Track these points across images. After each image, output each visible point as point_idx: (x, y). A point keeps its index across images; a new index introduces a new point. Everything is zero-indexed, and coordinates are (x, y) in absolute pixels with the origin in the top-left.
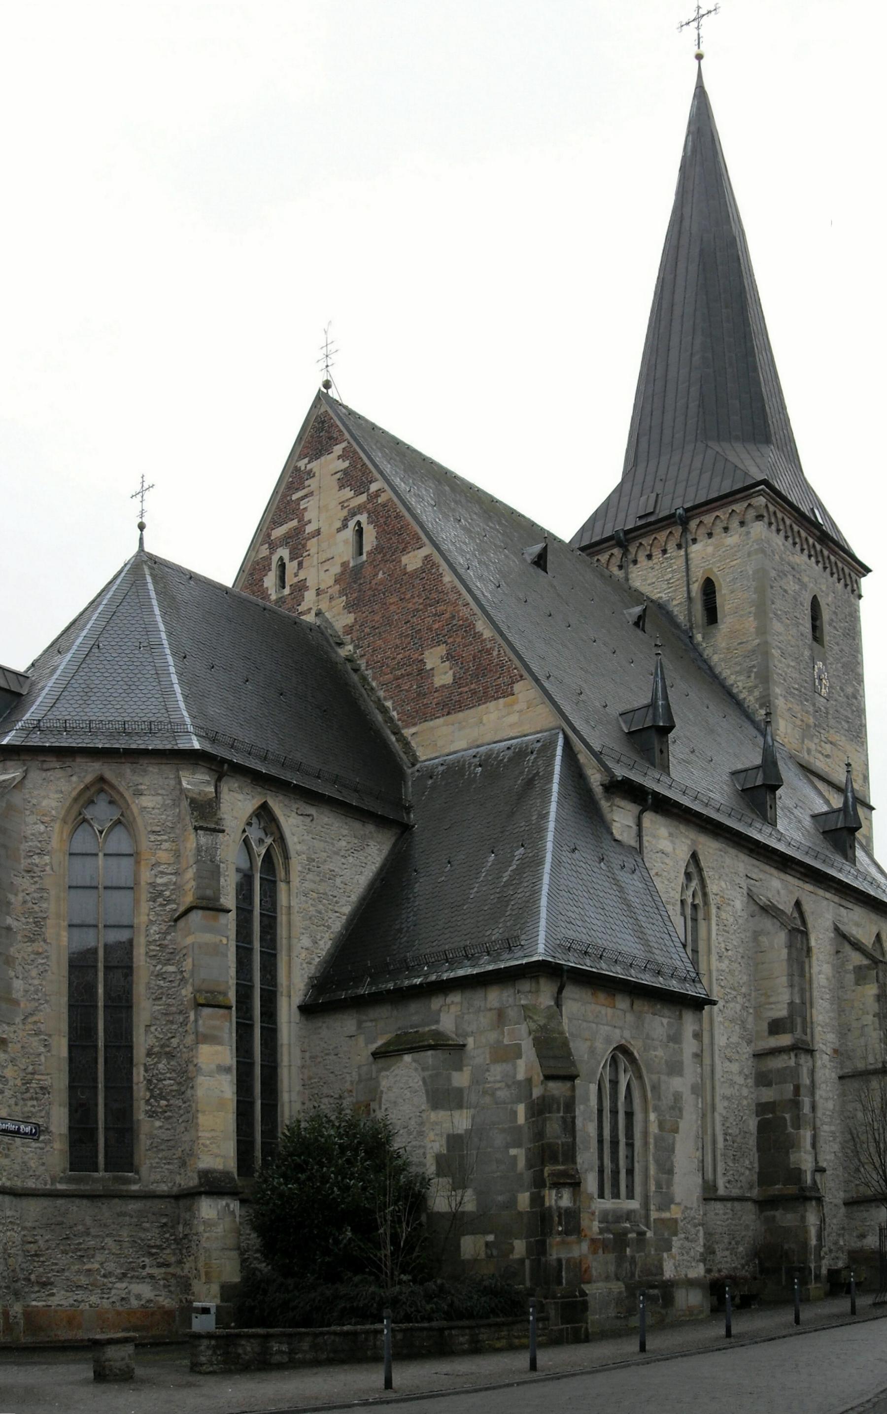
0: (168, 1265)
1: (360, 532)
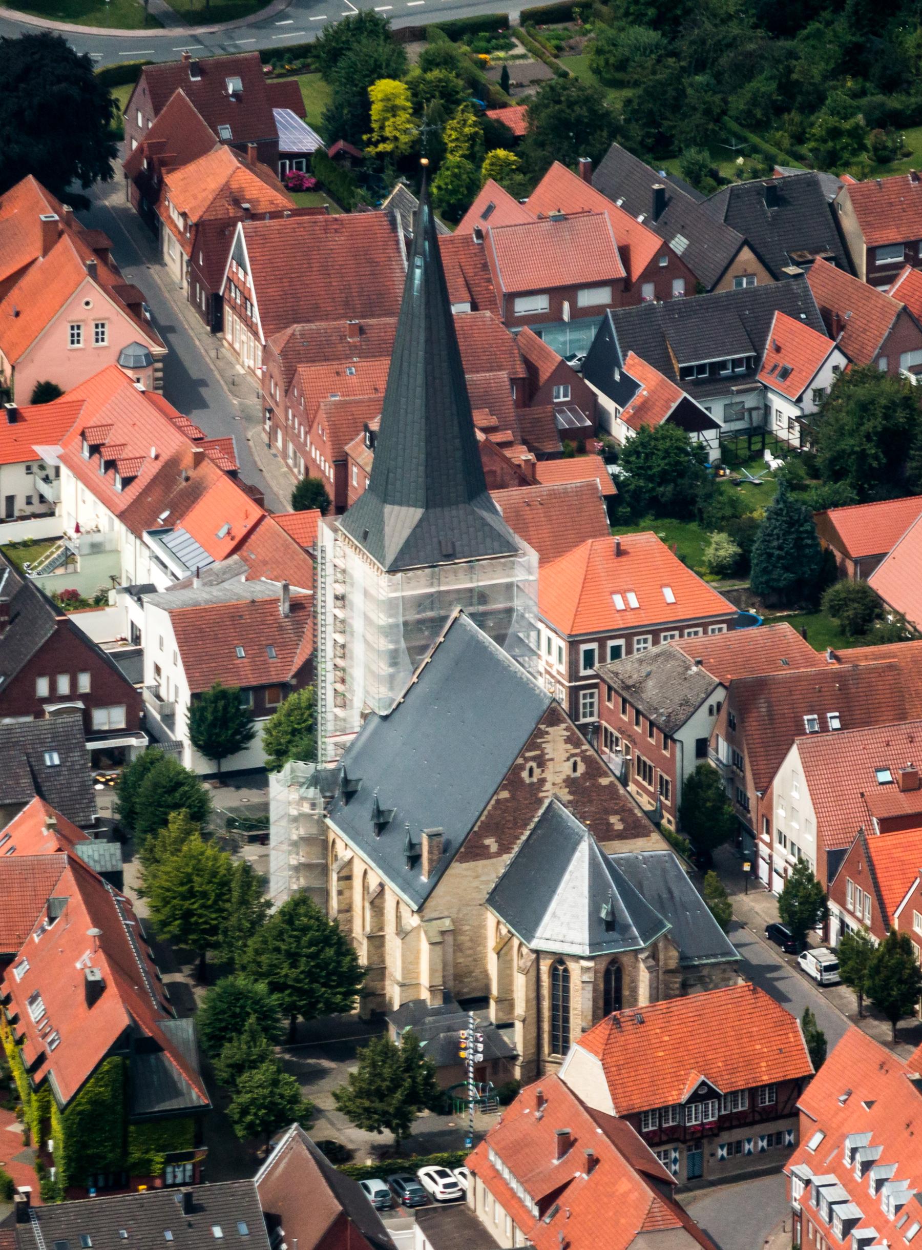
1: (575, 764)
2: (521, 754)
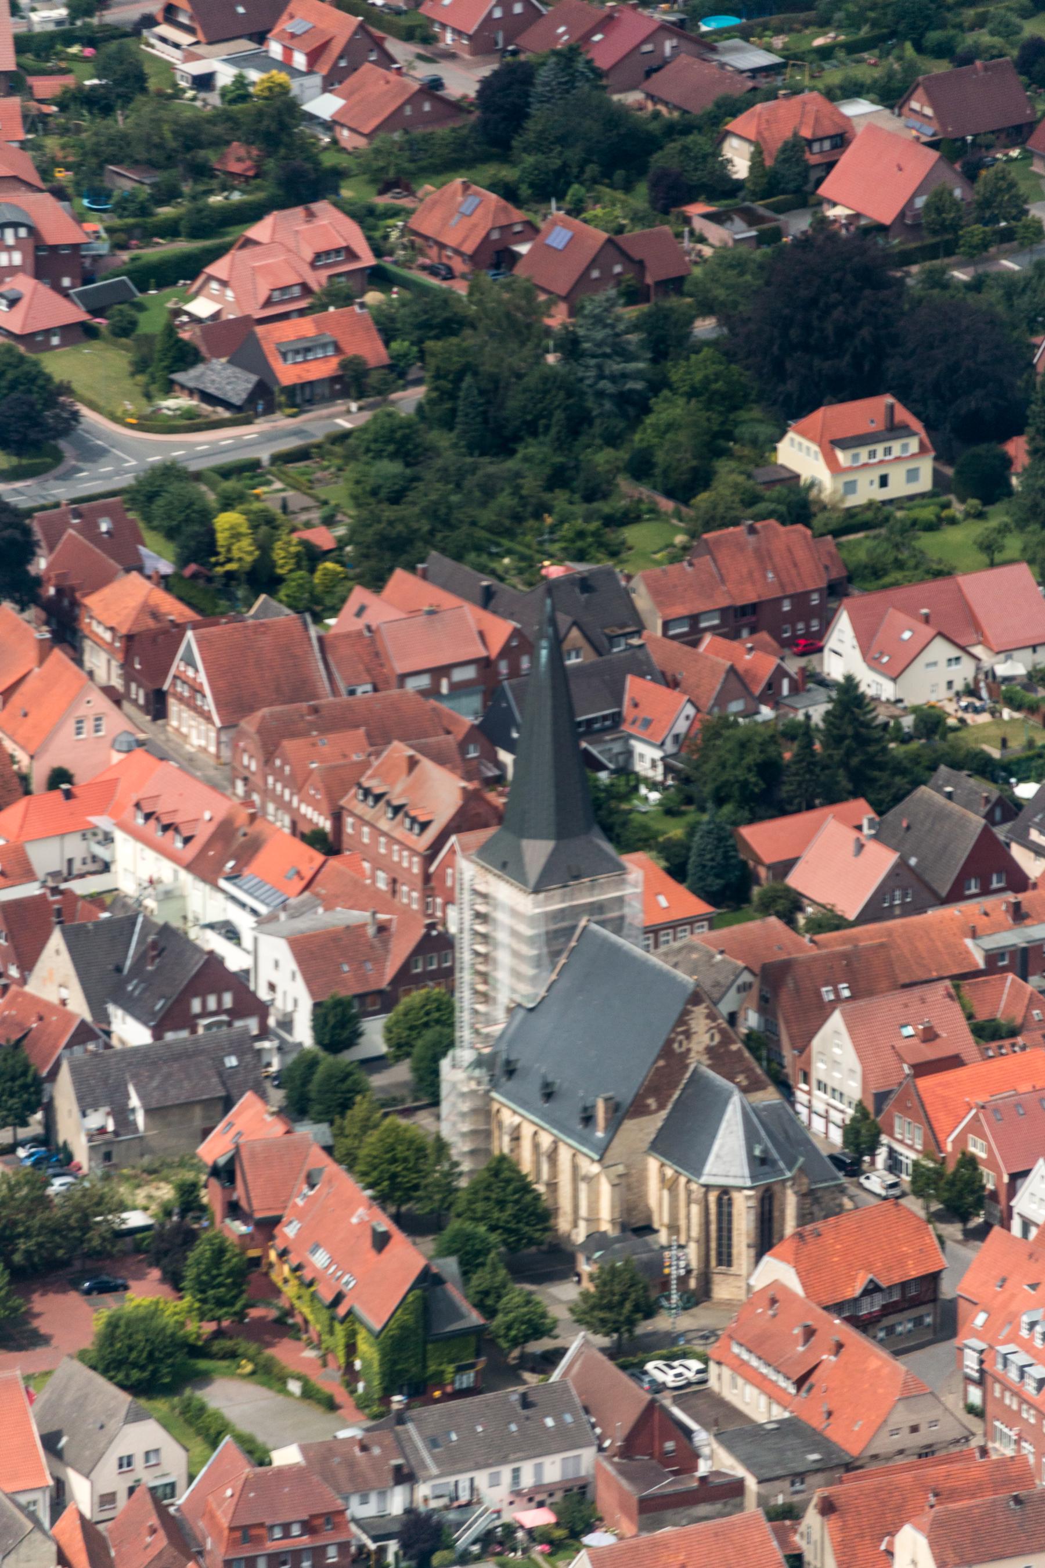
2: (673, 1030)
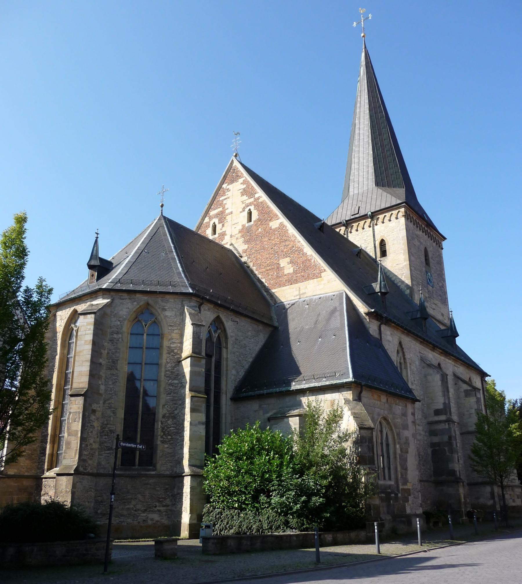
0: (168, 506)
1: (250, 213)
